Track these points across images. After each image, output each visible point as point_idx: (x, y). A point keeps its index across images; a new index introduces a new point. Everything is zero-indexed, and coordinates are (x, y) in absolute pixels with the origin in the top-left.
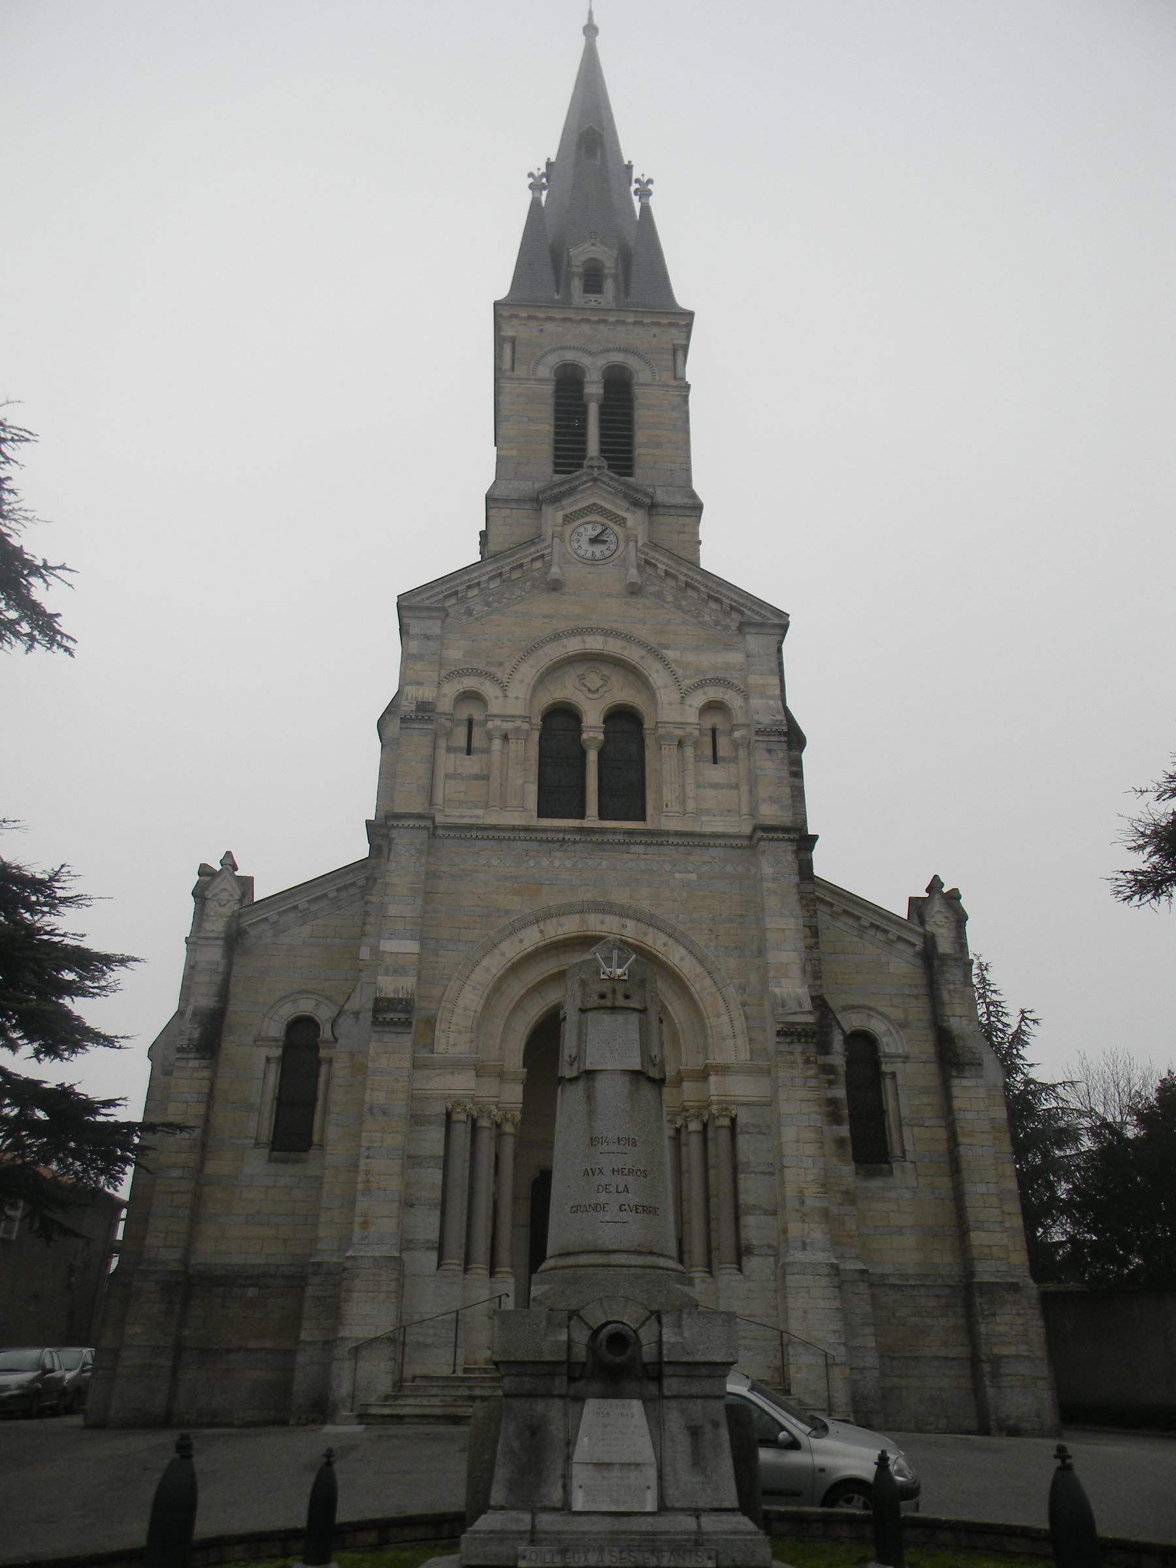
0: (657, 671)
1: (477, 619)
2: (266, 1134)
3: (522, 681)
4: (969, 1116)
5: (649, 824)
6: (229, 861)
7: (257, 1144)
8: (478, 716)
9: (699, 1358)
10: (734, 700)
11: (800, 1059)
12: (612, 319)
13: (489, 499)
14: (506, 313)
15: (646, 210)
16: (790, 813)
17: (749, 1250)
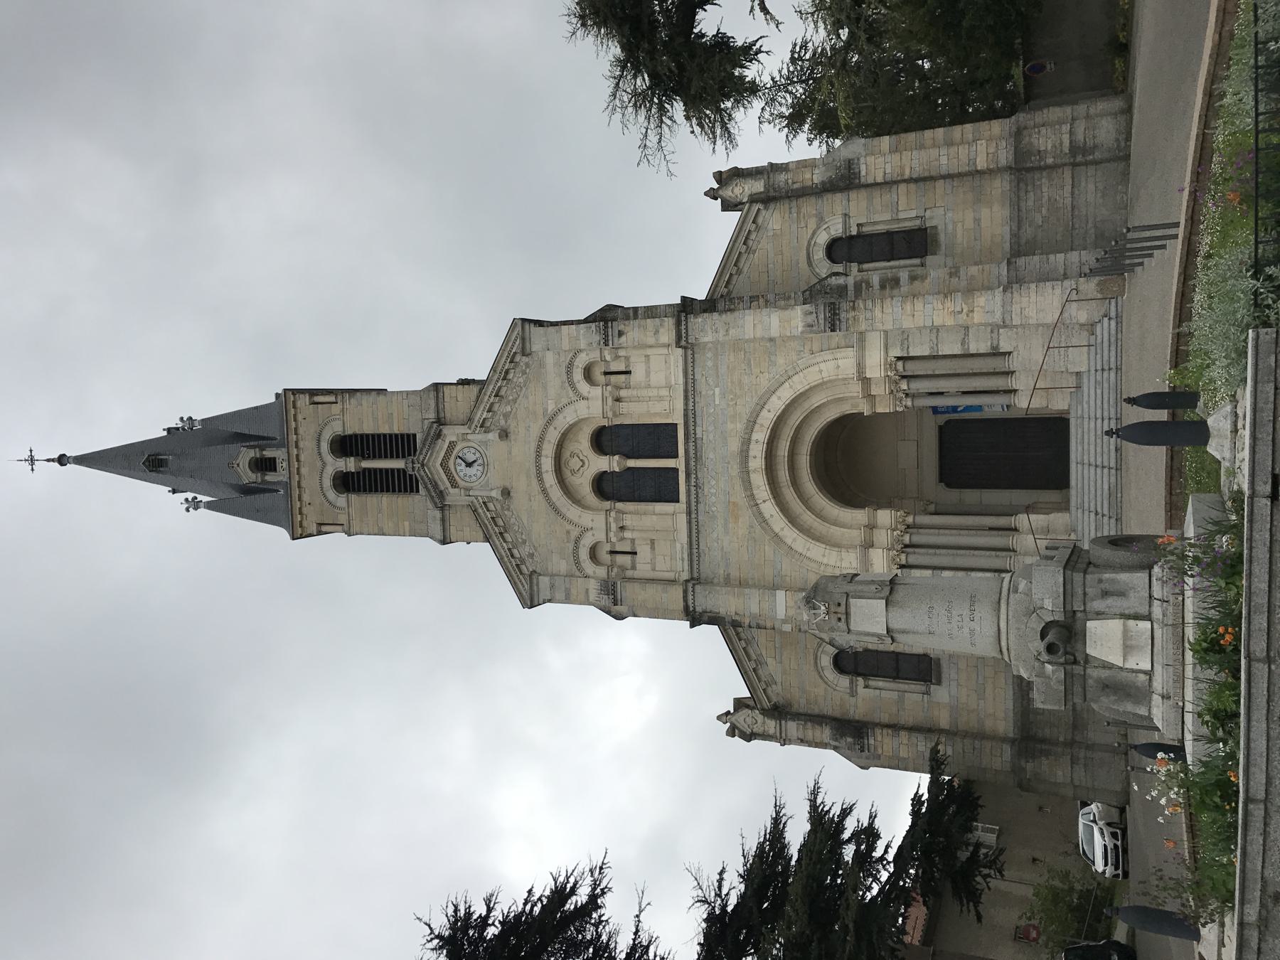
2: (920, 687)
5: (680, 421)
7: (928, 693)
8: (608, 548)
9: (1061, 590)
10: (582, 360)
11: (852, 314)
12: (295, 451)
13: (444, 542)
14: (300, 531)
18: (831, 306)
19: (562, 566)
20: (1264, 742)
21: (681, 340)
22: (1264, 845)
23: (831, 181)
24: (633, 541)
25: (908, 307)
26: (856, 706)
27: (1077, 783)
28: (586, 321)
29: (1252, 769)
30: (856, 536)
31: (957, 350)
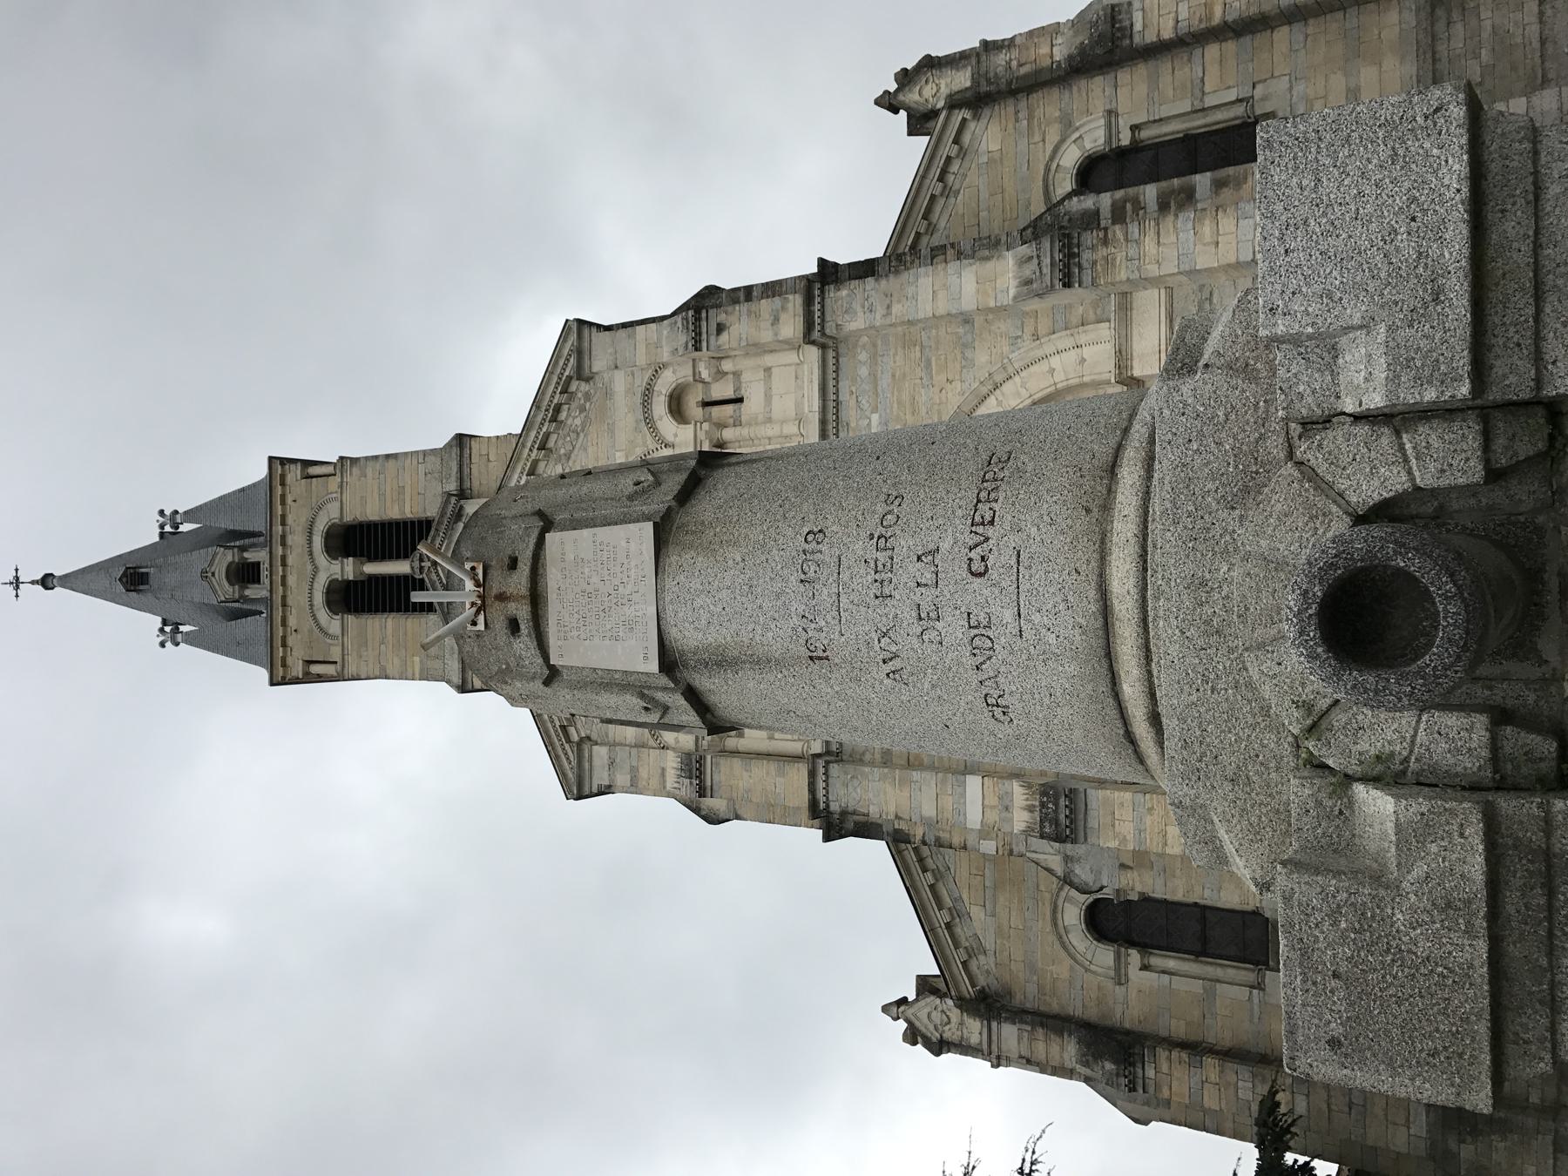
2: (1246, 974)
4: (1183, 15)
6: (897, 1008)
7: (1260, 986)
9: (1454, 247)
12: (280, 551)
13: (463, 688)
15: (190, 515)
16: (791, 297)
18: (1063, 242)
21: (814, 331)
23: (1082, 49)
25: (1207, 229)
26: (1126, 1003)
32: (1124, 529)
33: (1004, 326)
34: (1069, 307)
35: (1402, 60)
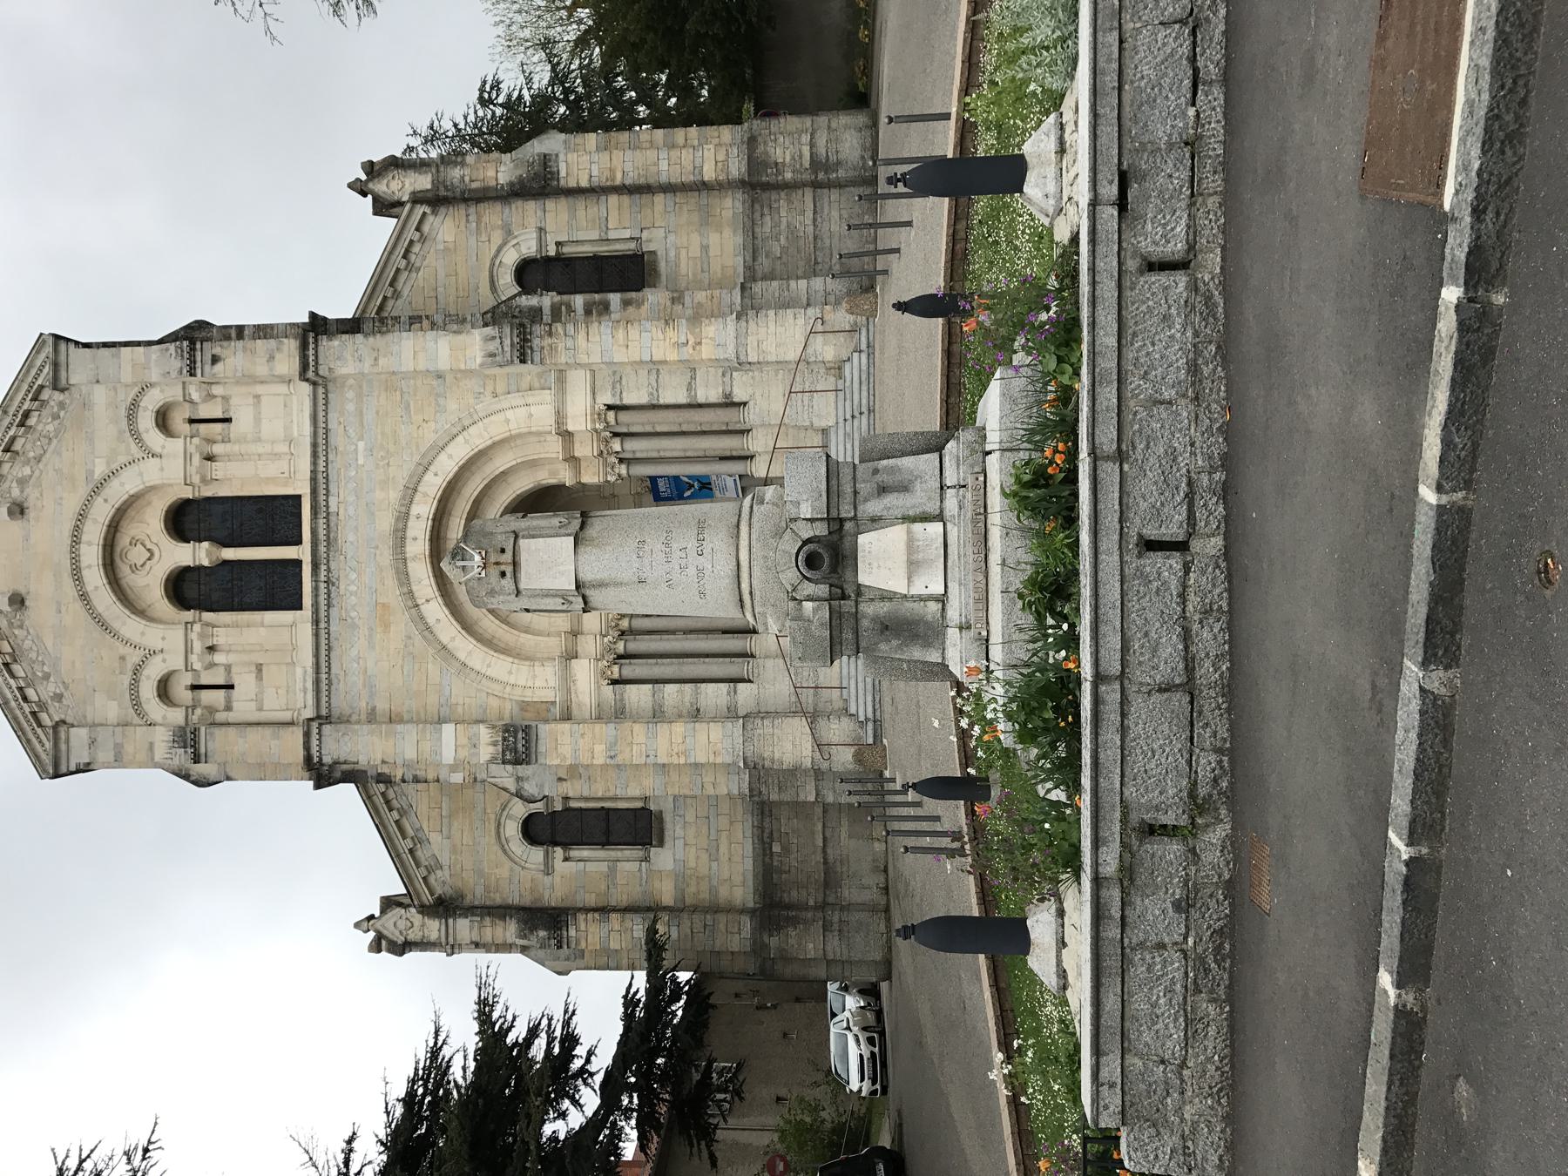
0: (122, 484)
1: (66, 688)
2: (634, 852)
3: (143, 634)
5: (302, 488)
7: (646, 859)
8: (188, 679)
9: (824, 487)
11: (548, 341)
17: (728, 396)
19: (112, 710)
20: (1118, 585)
21: (307, 370)
22: (1122, 748)
23: (521, 180)
24: (228, 668)
25: (621, 334)
27: (830, 956)
28: (161, 342)
29: (1103, 629)
30: (556, 645)
31: (682, 399)
32: (744, 543)
33: (472, 384)
34: (520, 375)
35: (735, 232)
